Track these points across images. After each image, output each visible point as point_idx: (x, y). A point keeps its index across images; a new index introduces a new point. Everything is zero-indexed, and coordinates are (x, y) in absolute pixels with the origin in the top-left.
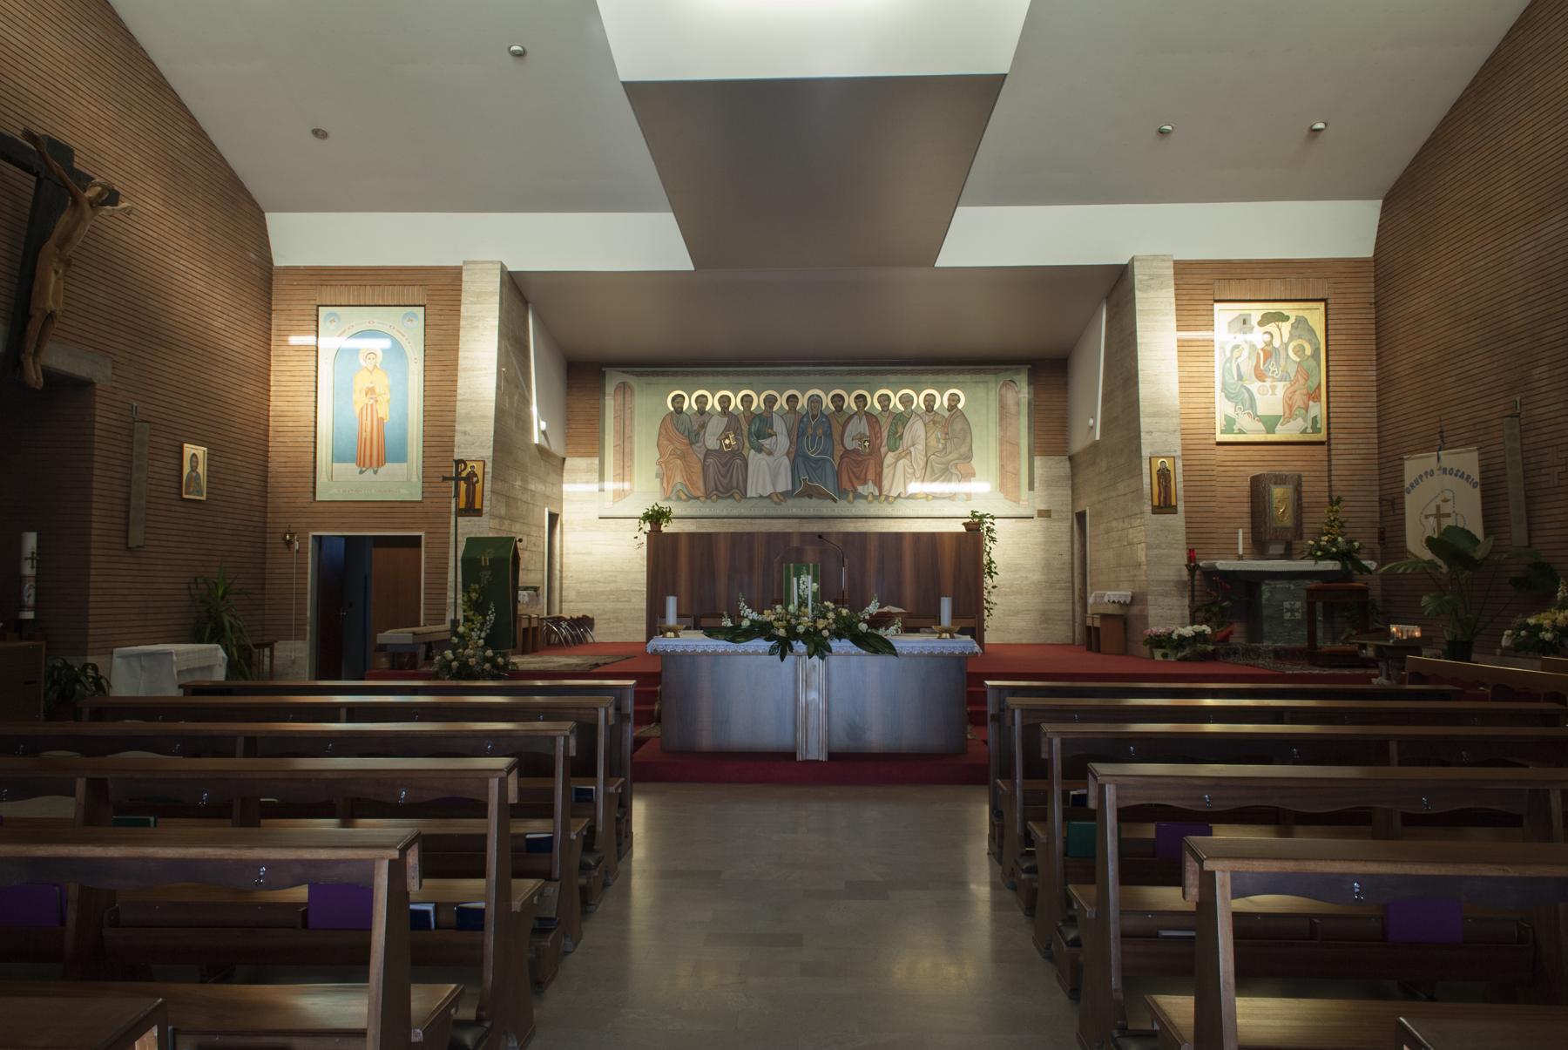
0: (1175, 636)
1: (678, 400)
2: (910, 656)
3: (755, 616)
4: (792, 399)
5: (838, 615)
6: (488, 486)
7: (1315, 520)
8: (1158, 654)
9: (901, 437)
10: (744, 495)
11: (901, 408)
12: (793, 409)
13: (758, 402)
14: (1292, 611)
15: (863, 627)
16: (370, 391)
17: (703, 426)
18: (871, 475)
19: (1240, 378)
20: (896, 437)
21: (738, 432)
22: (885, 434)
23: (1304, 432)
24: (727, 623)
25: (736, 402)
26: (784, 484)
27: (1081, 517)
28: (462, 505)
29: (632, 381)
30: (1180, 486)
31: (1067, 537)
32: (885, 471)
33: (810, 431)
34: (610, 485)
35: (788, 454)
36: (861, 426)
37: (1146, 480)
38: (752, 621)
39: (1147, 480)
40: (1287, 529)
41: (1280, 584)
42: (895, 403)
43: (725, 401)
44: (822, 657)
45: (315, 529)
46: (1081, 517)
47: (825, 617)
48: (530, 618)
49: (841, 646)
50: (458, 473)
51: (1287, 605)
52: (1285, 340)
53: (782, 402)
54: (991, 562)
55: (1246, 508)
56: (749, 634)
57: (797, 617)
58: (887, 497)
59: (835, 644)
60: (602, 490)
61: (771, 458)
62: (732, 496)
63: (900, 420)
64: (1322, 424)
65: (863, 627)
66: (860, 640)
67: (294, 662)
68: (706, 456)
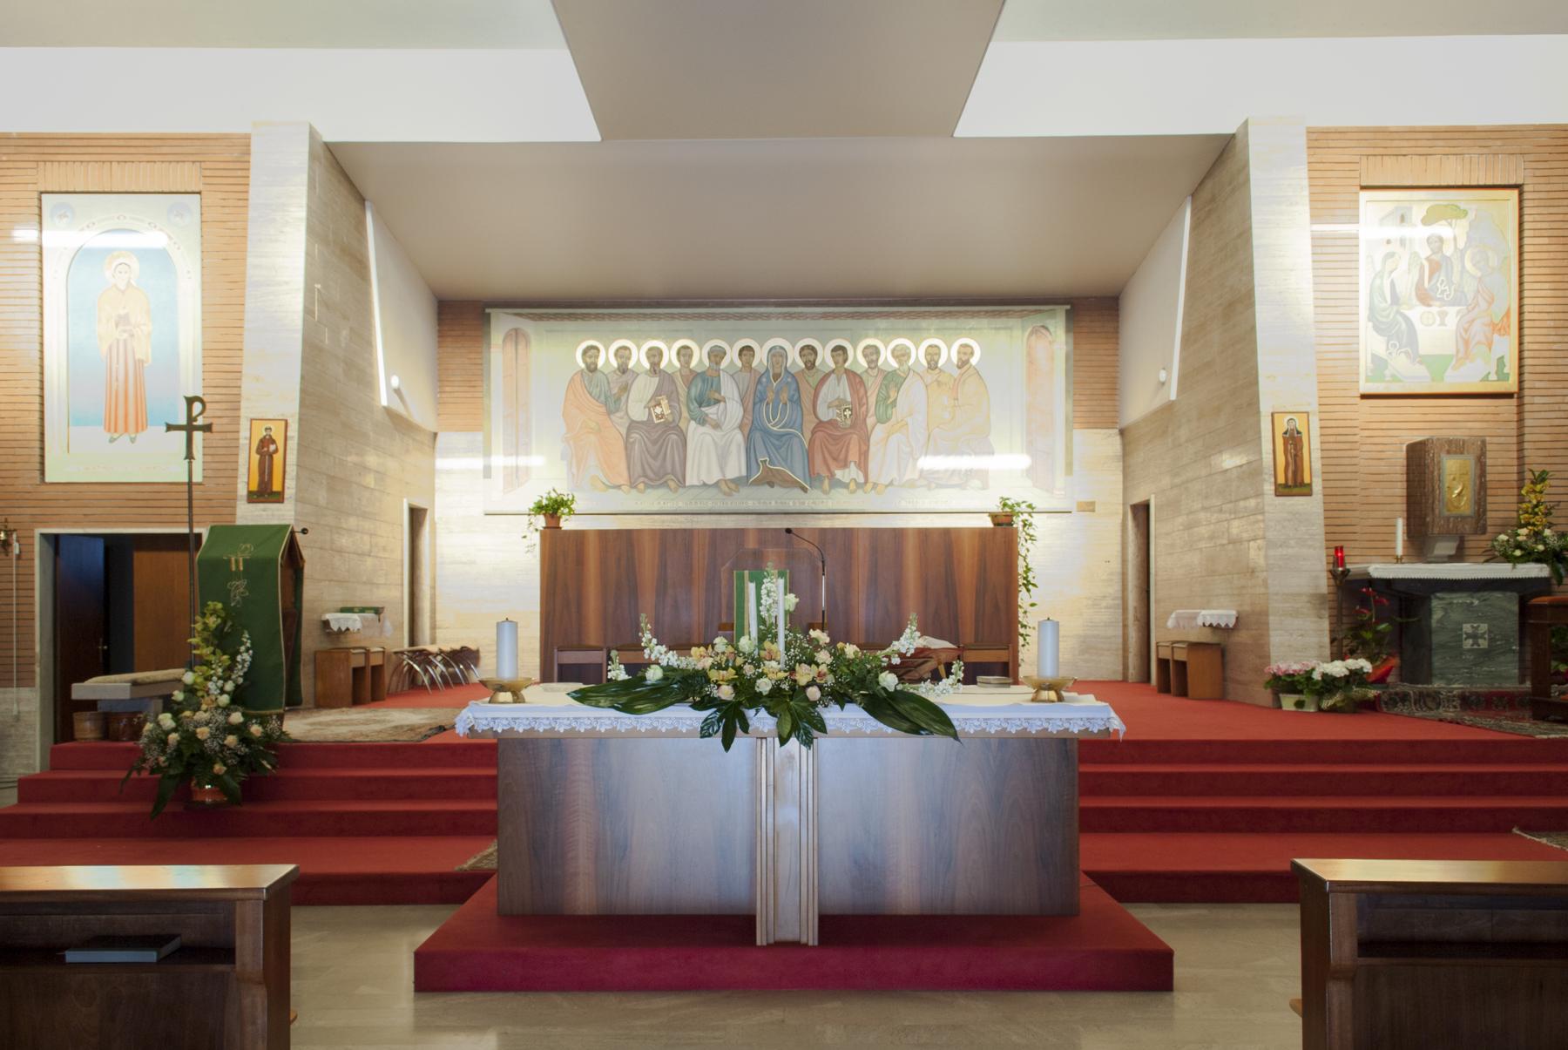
0: (1316, 676)
1: (590, 351)
2: (984, 739)
3: (672, 658)
4: (746, 351)
5: (838, 656)
6: (292, 458)
7: (1501, 506)
8: (1288, 702)
9: (894, 404)
10: (681, 482)
11: (895, 364)
12: (747, 366)
13: (700, 359)
14: (1474, 636)
15: (889, 680)
16: (122, 320)
17: (626, 388)
18: (853, 455)
19: (1396, 299)
20: (887, 403)
21: (672, 397)
22: (872, 400)
23: (1485, 379)
24: (618, 673)
25: (670, 359)
26: (736, 467)
27: (1142, 512)
28: (254, 487)
29: (528, 326)
30: (1316, 455)
31: (1117, 538)
32: (872, 449)
33: (771, 396)
34: (499, 461)
35: (741, 427)
36: (843, 390)
37: (1267, 446)
38: (668, 669)
39: (1269, 450)
40: (1464, 518)
41: (1460, 598)
42: (887, 359)
43: (654, 355)
44: (808, 742)
45: (45, 524)
46: (1142, 512)
47: (811, 661)
48: (367, 653)
49: (846, 719)
50: (191, 418)
51: (1467, 628)
52: (1461, 245)
53: (732, 355)
54: (1028, 570)
55: (1400, 489)
56: (660, 696)
57: (757, 662)
58: (875, 485)
59: (831, 714)
60: (487, 472)
61: (718, 433)
62: (665, 485)
63: (892, 380)
64: (1511, 368)
65: (889, 680)
66: (882, 706)
67: (17, 718)
68: (629, 429)
